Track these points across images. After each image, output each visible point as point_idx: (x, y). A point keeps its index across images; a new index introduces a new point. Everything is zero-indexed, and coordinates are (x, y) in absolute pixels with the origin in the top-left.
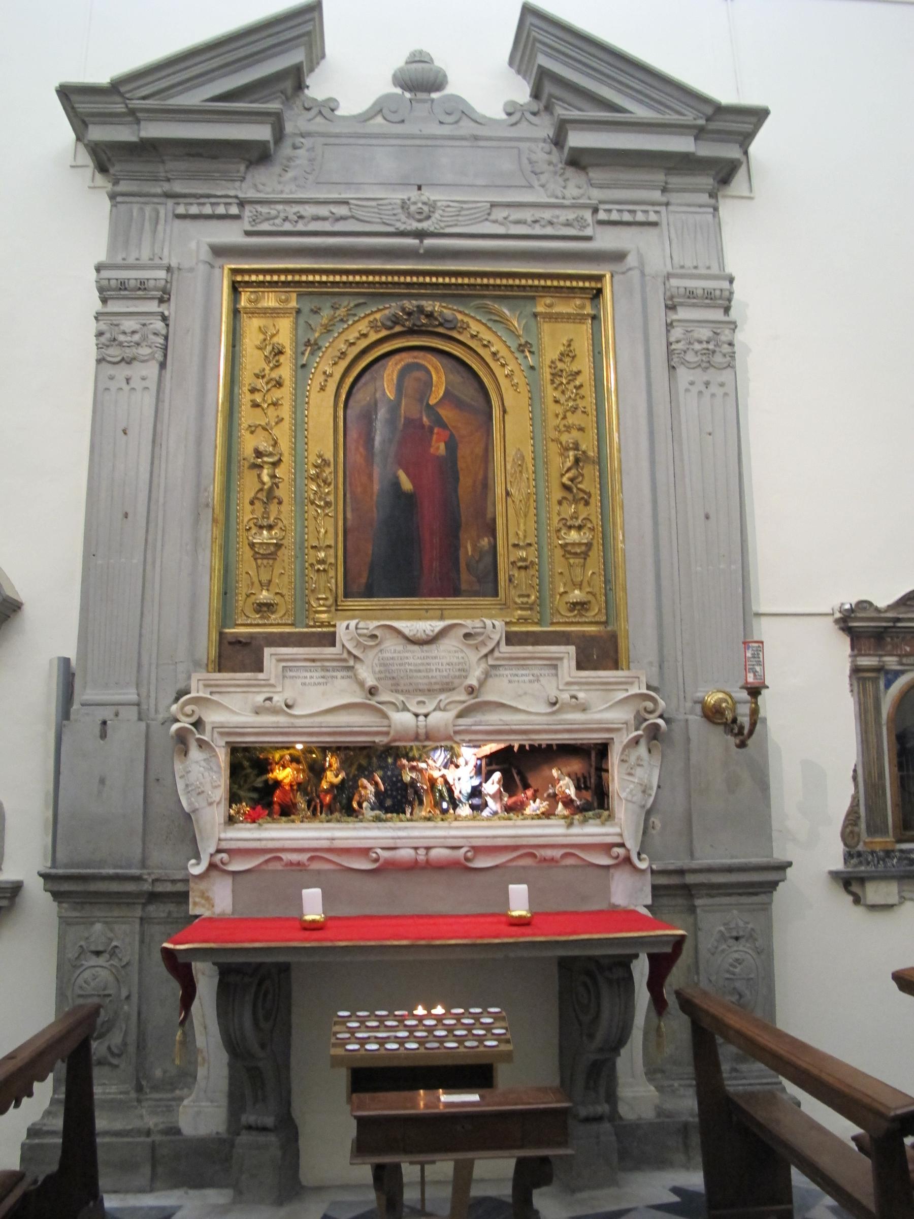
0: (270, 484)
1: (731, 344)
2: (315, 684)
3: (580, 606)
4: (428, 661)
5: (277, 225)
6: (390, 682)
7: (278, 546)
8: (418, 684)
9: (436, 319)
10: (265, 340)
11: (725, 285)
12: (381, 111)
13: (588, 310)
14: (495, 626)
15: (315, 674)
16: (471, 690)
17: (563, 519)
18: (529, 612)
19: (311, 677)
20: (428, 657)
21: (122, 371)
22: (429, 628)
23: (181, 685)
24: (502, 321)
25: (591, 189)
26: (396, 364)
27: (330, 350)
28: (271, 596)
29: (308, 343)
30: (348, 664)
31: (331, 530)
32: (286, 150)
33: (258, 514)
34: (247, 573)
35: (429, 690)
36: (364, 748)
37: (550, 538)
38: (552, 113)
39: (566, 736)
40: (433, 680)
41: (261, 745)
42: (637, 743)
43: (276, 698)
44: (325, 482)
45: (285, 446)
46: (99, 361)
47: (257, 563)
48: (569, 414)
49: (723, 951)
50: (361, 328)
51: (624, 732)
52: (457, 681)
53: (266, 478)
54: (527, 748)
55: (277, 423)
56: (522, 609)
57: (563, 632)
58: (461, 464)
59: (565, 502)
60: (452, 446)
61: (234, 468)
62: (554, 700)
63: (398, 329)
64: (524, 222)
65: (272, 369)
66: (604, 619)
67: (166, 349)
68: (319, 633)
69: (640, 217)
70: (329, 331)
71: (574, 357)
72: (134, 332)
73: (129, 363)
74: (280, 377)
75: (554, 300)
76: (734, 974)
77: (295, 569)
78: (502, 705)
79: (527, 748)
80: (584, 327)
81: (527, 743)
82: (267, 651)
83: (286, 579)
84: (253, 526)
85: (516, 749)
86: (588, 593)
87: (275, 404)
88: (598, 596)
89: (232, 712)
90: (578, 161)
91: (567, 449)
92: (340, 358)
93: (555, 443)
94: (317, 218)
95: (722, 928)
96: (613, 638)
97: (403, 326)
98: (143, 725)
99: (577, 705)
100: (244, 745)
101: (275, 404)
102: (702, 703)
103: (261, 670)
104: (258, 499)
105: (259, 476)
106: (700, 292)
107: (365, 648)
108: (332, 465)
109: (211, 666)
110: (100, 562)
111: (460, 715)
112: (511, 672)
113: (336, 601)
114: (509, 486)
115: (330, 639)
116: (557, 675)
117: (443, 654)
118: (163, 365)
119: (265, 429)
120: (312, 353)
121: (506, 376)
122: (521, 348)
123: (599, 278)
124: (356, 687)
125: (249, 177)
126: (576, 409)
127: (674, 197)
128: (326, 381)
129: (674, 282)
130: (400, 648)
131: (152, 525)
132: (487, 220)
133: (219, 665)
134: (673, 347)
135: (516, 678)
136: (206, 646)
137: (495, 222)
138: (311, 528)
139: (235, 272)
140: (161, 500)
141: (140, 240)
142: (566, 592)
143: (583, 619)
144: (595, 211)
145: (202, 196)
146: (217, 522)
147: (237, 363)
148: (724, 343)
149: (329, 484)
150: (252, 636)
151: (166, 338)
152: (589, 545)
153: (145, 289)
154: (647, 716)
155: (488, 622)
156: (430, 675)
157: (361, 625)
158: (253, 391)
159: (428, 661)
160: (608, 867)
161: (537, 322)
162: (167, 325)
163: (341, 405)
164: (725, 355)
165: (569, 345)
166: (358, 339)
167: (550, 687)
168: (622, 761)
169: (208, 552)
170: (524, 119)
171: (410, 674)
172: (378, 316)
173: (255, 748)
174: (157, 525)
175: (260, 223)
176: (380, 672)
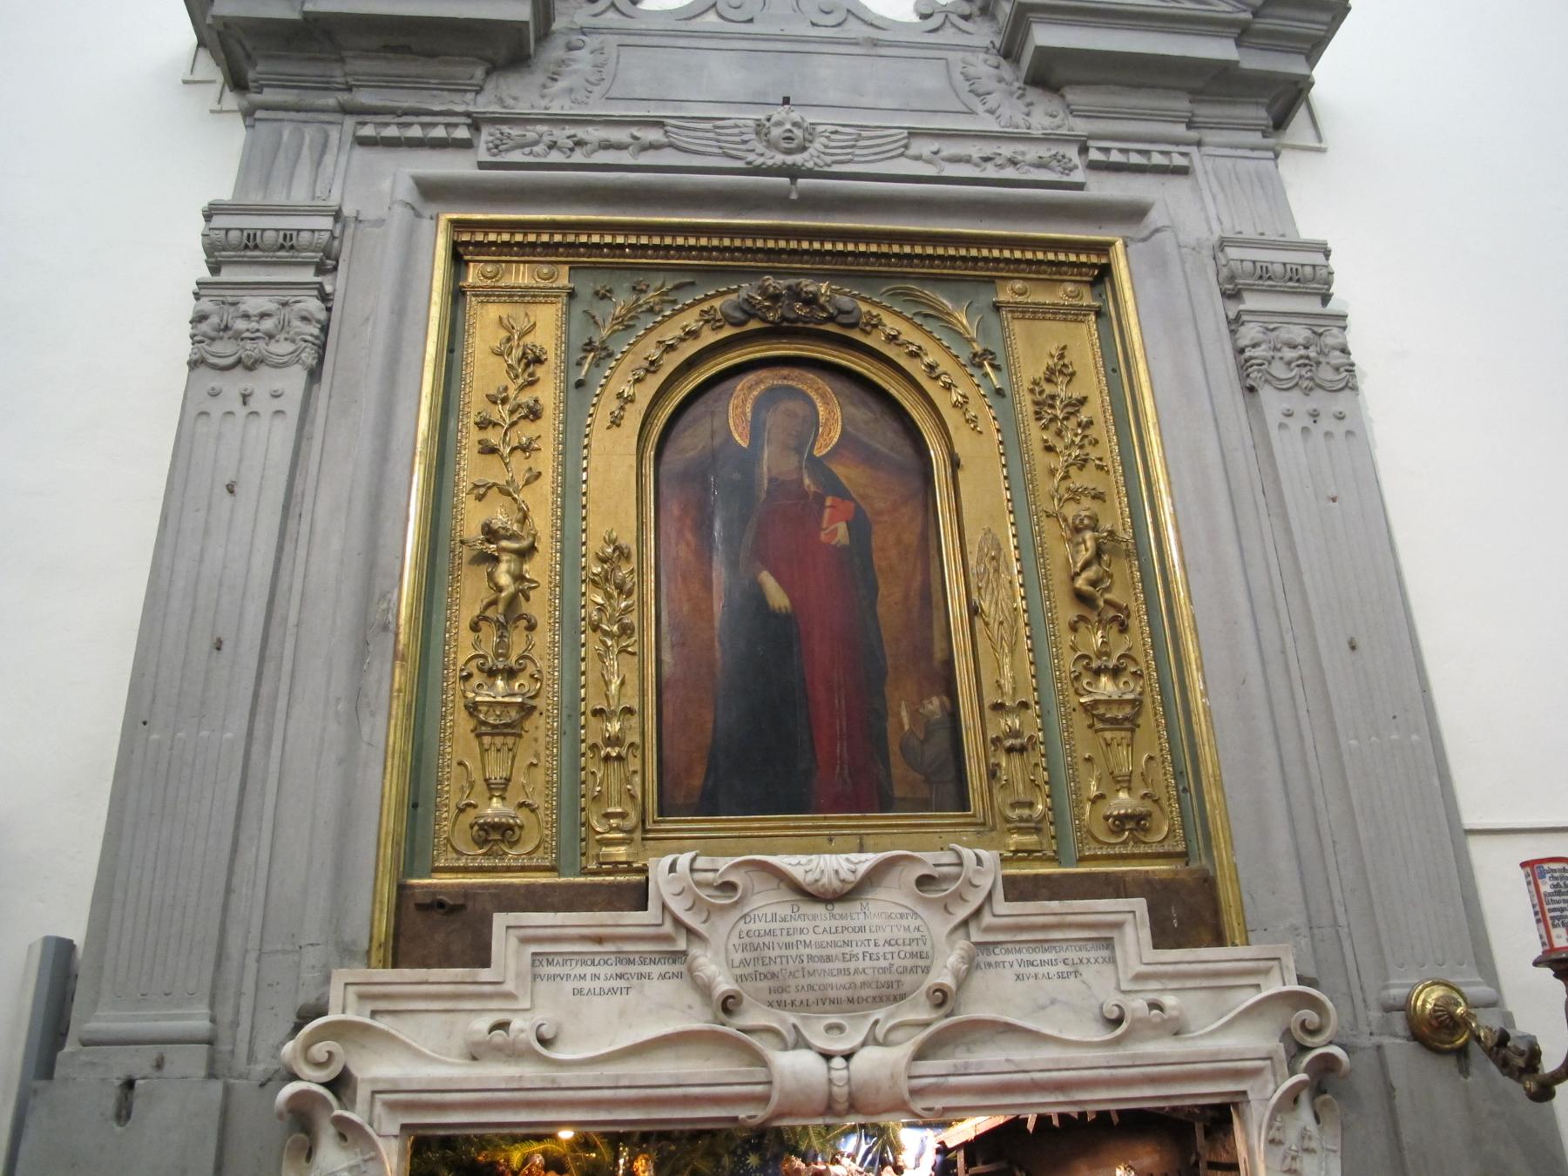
0: (512, 589)
1: (1345, 351)
2: (602, 992)
3: (1134, 823)
4: (847, 936)
5: (538, 155)
6: (765, 984)
7: (527, 710)
8: (824, 987)
9: (823, 309)
10: (509, 340)
11: (1318, 258)
12: (714, 5)
13: (1087, 300)
14: (983, 864)
15: (603, 970)
16: (941, 998)
17: (1083, 657)
18: (1034, 838)
19: (596, 977)
20: (845, 929)
21: (233, 384)
22: (846, 866)
23: (307, 997)
25: (1071, 119)
26: (750, 388)
27: (630, 357)
28: (511, 811)
29: (589, 347)
30: (673, 948)
31: (633, 680)
32: (555, 51)
33: (488, 648)
34: (460, 764)
35: (851, 1001)
36: (697, 1135)
37: (1062, 691)
38: (993, 17)
39: (1148, 1091)
40: (860, 978)
41: (478, 1131)
42: (1296, 1101)
43: (517, 1023)
44: (620, 587)
45: (542, 522)
46: (194, 364)
47: (481, 744)
48: (1073, 471)
50: (688, 324)
51: (1268, 1075)
52: (908, 979)
53: (504, 579)
54: (1056, 1122)
55: (527, 483)
56: (1020, 831)
57: (1107, 874)
58: (879, 561)
59: (1082, 626)
60: (860, 527)
61: (443, 563)
62: (1115, 1014)
63: (753, 325)
64: (967, 160)
65: (521, 388)
66: (1181, 848)
67: (322, 347)
68: (611, 885)
69: (1157, 159)
70: (628, 327)
71: (1073, 374)
73: (250, 368)
74: (536, 401)
75: (1028, 285)
77: (559, 755)
78: (1009, 1029)
79: (1056, 1122)
80: (1084, 327)
81: (1053, 1111)
82: (500, 920)
83: (540, 775)
84: (475, 671)
85: (1030, 1126)
86: (1145, 796)
87: (525, 448)
88: (1164, 802)
89: (418, 1055)
90: (1049, 74)
91: (1077, 530)
92: (647, 371)
93: (1052, 521)
94: (607, 146)
96: (1207, 884)
97: (764, 320)
98: (216, 1087)
99: (1164, 1021)
100: (442, 1133)
101: (525, 448)
102: (1406, 1007)
103: (486, 963)
104: (486, 619)
105: (491, 576)
106: (1279, 269)
107: (711, 911)
108: (634, 558)
109: (376, 955)
110: (155, 736)
111: (920, 1055)
112: (1019, 956)
113: (643, 822)
114: (975, 597)
115: (638, 897)
116: (1113, 960)
117: (877, 921)
118: (314, 374)
119: (504, 492)
120: (597, 364)
121: (955, 406)
122: (977, 361)
123: (1104, 248)
124: (693, 998)
125: (490, 86)
126: (1085, 461)
127: (1209, 136)
128: (622, 408)
129: (1233, 253)
130: (785, 910)
131: (270, 667)
132: (902, 155)
133: (395, 955)
134: (1248, 354)
135: (1032, 970)
136: (369, 911)
137: (918, 158)
138: (593, 676)
139: (458, 225)
140: (292, 619)
141: (291, 176)
142: (1101, 797)
143: (1142, 849)
144: (1084, 150)
145: (406, 113)
146: (403, 659)
147: (455, 377)
148: (1334, 348)
149: (629, 594)
150: (468, 893)
151: (325, 329)
152: (1137, 703)
153: (292, 247)
154: (1309, 1041)
155: (967, 853)
156: (852, 965)
157: (702, 862)
158: (484, 424)
159: (847, 936)
161: (1001, 321)
162: (329, 310)
163: (650, 453)
164: (1337, 369)
165: (1062, 356)
166: (682, 340)
167: (1102, 986)
168: (1272, 1141)
169: (381, 720)
170: (948, 24)
171: (811, 966)
172: (717, 303)
173: (467, 1138)
174: (279, 669)
175: (507, 150)
176: (744, 963)
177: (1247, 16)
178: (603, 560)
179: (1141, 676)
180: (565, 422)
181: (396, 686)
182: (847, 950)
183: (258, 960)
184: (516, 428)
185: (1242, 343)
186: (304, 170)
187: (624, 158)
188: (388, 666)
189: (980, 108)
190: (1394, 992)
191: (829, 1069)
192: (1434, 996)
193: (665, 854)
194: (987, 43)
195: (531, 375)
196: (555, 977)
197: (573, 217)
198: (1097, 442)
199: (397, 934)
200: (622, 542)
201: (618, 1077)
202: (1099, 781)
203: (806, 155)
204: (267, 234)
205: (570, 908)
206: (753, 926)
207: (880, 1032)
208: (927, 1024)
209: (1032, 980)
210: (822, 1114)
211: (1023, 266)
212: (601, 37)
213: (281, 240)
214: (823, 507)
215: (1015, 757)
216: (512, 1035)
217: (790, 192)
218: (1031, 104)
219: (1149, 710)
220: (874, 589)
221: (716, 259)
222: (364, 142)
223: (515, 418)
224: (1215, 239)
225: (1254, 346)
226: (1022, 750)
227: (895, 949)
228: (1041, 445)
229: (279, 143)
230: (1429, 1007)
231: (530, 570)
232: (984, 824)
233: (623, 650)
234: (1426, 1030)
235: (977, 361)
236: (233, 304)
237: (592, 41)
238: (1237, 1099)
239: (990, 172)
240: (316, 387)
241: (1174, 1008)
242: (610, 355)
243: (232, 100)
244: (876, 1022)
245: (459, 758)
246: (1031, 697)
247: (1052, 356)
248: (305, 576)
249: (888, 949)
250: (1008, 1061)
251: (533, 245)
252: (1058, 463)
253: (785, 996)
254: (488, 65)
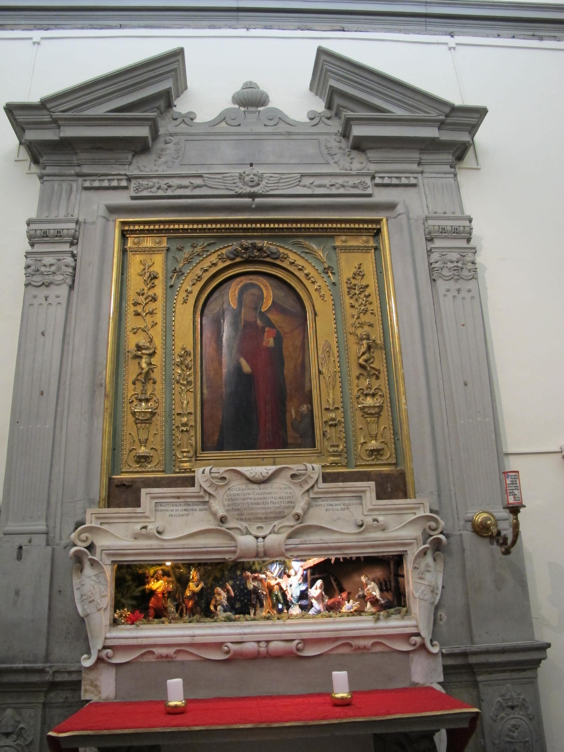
0: (147, 369)
2: (179, 515)
3: (376, 453)
4: (265, 496)
5: (153, 192)
6: (236, 513)
7: (153, 414)
8: (257, 513)
9: (265, 252)
10: (144, 269)
12: (225, 119)
13: (372, 243)
16: (298, 517)
23: (79, 518)
25: (369, 164)
26: (238, 284)
27: (190, 274)
31: (192, 401)
32: (160, 144)
33: (139, 391)
34: (130, 434)
35: (266, 518)
38: (340, 118)
40: (269, 511)
43: (150, 526)
44: (187, 367)
45: (158, 342)
46: (27, 285)
47: (137, 427)
48: (361, 315)
49: (502, 718)
50: (213, 260)
52: (286, 511)
53: (144, 365)
54: (341, 560)
55: (152, 327)
56: (333, 456)
57: (365, 472)
58: (285, 353)
62: (360, 523)
63: (238, 260)
64: (325, 186)
65: (149, 289)
66: (394, 461)
67: (74, 276)
68: (184, 477)
69: (404, 181)
70: (190, 262)
71: (364, 275)
72: (51, 265)
75: (347, 237)
76: (512, 738)
78: (321, 528)
79: (341, 560)
80: (369, 255)
81: (341, 557)
82: (144, 491)
83: (158, 438)
84: (134, 400)
85: (333, 562)
88: (389, 444)
89: (116, 537)
90: (360, 146)
91: (362, 339)
92: (197, 280)
94: (180, 187)
95: (500, 699)
96: (402, 475)
97: (242, 257)
98: (49, 549)
100: (125, 563)
101: (151, 313)
102: (472, 521)
103: (139, 506)
104: (138, 380)
107: (217, 487)
109: (102, 503)
111: (290, 537)
112: (327, 502)
114: (320, 367)
115: (190, 482)
116: (362, 504)
117: (275, 490)
118: (71, 287)
120: (178, 278)
122: (326, 271)
123: (378, 222)
124: (211, 518)
125: (134, 161)
126: (366, 311)
127: (426, 168)
128: (187, 296)
129: (430, 222)
130: (244, 487)
132: (298, 185)
133: (108, 503)
134: (433, 266)
135: (332, 507)
136: (99, 488)
137: (304, 186)
139: (123, 223)
140: (68, 382)
142: (365, 443)
143: (379, 462)
144: (373, 178)
146: (108, 397)
148: (469, 262)
149: (190, 369)
150: (133, 481)
151: (74, 269)
152: (381, 408)
153: (60, 236)
154: (432, 533)
155: (309, 466)
156: (267, 506)
157: (214, 470)
158: (136, 304)
159: (265, 496)
162: (76, 260)
163: (199, 313)
164: (470, 270)
165: (359, 268)
166: (210, 267)
167: (357, 513)
170: (321, 122)
172: (224, 251)
173: (136, 565)
175: (141, 191)
176: (229, 505)
177: (443, 117)
178: (181, 356)
179: (383, 396)
180: (166, 302)
181: (106, 407)
182: (265, 500)
183: (62, 505)
184: (148, 305)
185: (432, 261)
186: (64, 201)
187: (187, 192)
188: (103, 400)
189: (332, 162)
190: (469, 515)
191: (257, 542)
192: (482, 517)
193: (201, 467)
194: (336, 131)
195: (153, 284)
196: (163, 510)
197: (168, 219)
198: (371, 303)
199: (109, 495)
200: (187, 349)
201: (184, 545)
202: (364, 437)
203: (259, 187)
204: (51, 231)
205: (169, 486)
206: (232, 492)
207: (276, 529)
208: (293, 526)
209: (331, 511)
210: (255, 557)
211: (346, 230)
212: (178, 137)
213: (56, 234)
214: (264, 332)
215: (333, 428)
216: (148, 531)
217: (252, 205)
218: (353, 158)
219: (386, 410)
220: (283, 364)
221: (224, 233)
222: (86, 189)
223: (147, 301)
224: (424, 216)
225: (436, 262)
226: (335, 425)
227: (281, 500)
228: (350, 305)
229: (53, 190)
230: (479, 520)
231: (154, 361)
232: (321, 453)
233: (188, 390)
234: (478, 529)
235: (326, 271)
236: (40, 261)
237: (174, 139)
238: (403, 553)
239: (334, 191)
240: (72, 292)
241: (382, 521)
242: (183, 274)
243: (35, 169)
244: (275, 526)
245: (129, 432)
246: (339, 405)
247: (356, 268)
248: (72, 366)
249: (279, 500)
250: (321, 539)
251: (153, 230)
252: (355, 312)
253: (243, 517)
254: (133, 153)
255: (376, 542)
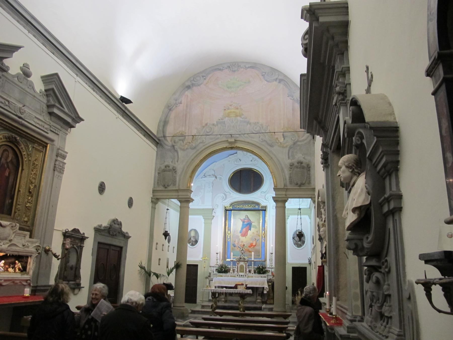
24: (28, 146)
90: (51, 114)
102: (45, 248)
129: (60, 151)
160: (25, 285)
167: (23, 241)
255: (19, 249)
